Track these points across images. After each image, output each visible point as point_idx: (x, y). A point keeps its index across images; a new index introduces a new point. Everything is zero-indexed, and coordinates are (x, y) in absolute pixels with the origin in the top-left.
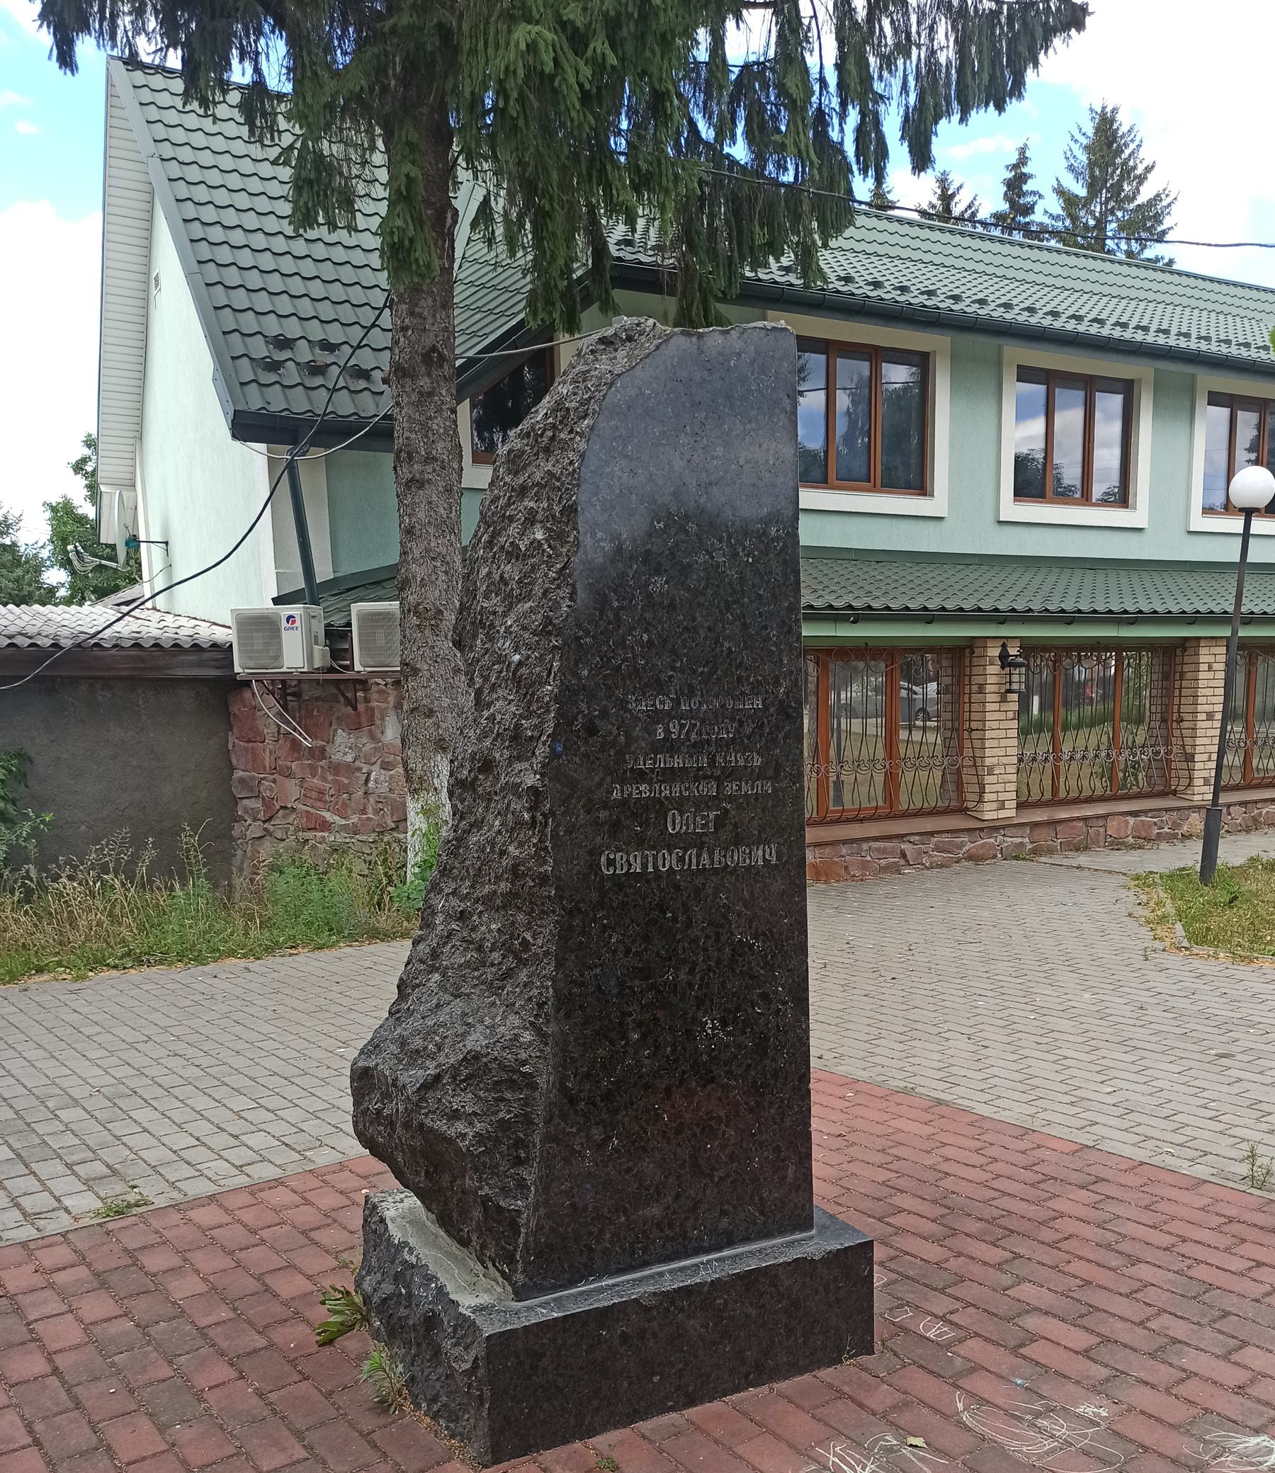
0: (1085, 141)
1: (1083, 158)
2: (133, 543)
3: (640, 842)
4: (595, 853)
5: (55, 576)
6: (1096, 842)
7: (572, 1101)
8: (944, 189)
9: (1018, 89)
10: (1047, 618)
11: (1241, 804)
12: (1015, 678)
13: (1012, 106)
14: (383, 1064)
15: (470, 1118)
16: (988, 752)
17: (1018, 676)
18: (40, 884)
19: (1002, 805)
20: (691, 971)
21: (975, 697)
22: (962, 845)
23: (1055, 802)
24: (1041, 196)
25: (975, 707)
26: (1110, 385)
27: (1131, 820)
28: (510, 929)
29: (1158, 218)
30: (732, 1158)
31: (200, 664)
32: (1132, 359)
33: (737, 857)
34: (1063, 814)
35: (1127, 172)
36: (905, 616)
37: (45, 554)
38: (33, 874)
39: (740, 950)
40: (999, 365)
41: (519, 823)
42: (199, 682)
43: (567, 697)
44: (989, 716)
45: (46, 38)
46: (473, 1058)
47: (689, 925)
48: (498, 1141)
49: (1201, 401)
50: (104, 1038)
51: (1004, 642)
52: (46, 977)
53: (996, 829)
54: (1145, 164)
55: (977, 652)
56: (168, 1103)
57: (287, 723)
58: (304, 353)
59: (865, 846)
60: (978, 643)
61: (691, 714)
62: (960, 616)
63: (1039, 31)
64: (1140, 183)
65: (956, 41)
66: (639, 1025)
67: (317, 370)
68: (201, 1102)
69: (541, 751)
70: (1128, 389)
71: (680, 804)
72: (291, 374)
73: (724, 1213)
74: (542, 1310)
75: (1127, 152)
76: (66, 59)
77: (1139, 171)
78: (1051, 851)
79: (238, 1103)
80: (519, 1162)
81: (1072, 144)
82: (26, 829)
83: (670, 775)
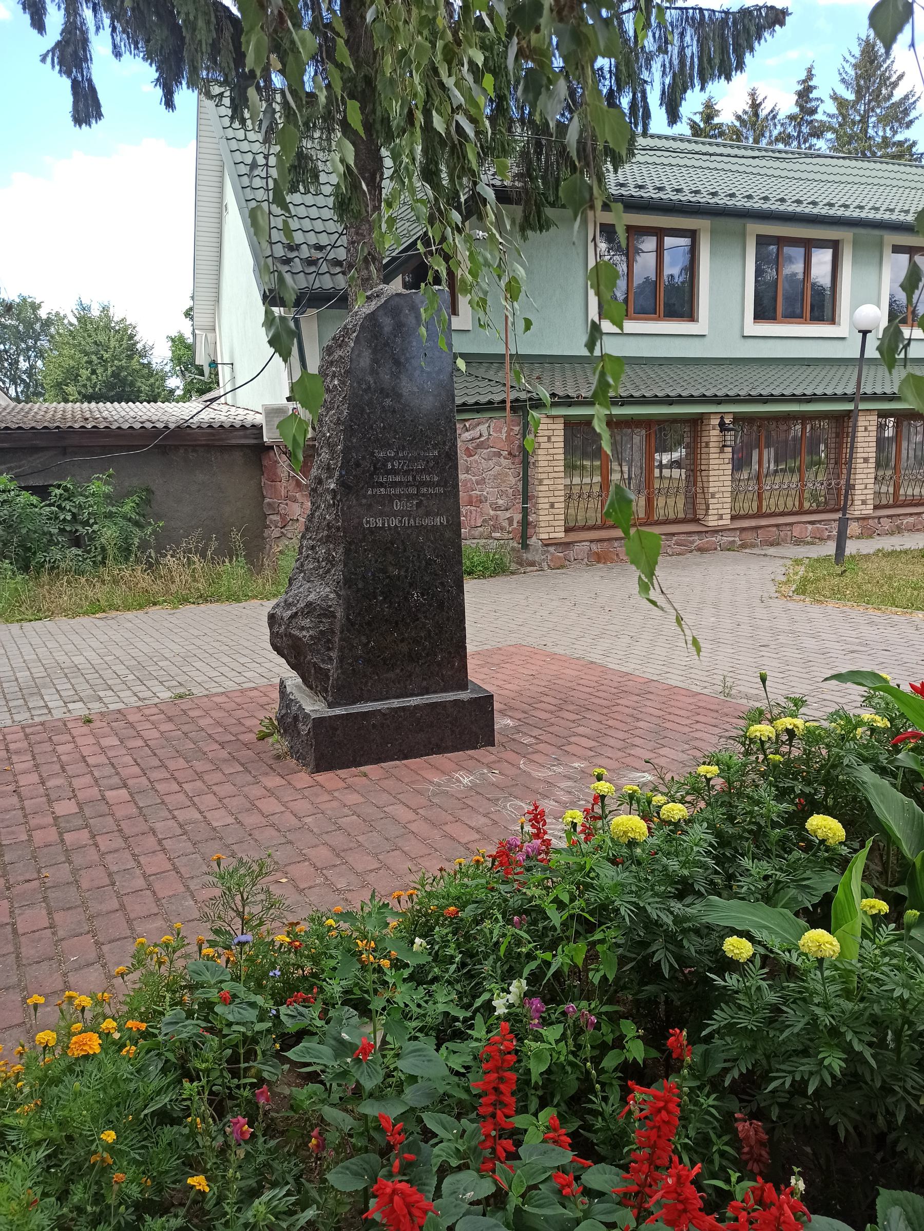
0: (853, 61)
1: (852, 72)
2: (214, 364)
3: (382, 514)
5: (175, 383)
6: (785, 541)
7: (353, 624)
8: (754, 100)
9: (740, 66)
10: (750, 399)
11: (888, 516)
12: (728, 438)
13: (737, 77)
14: (278, 611)
15: (308, 629)
16: (711, 484)
18: (157, 560)
19: (721, 517)
20: (406, 571)
21: (704, 450)
22: (694, 541)
23: (759, 515)
24: (822, 101)
25: (703, 456)
26: (822, 244)
27: (810, 527)
28: (328, 553)
29: (906, 112)
30: (427, 655)
31: (246, 437)
32: (835, 228)
34: (763, 522)
35: (884, 80)
36: (656, 401)
37: (167, 368)
38: (153, 555)
39: (429, 562)
40: (743, 236)
41: (329, 505)
42: (243, 447)
43: (346, 450)
44: (712, 462)
45: (159, 92)
46: (309, 604)
47: (405, 551)
48: (319, 639)
49: (887, 251)
50: (184, 634)
51: (722, 416)
52: (158, 607)
53: (717, 532)
54: (898, 74)
55: (705, 422)
56: (210, 660)
57: (293, 470)
58: (305, 252)
61: (404, 458)
63: (753, 29)
64: (894, 88)
65: (698, 41)
66: (382, 593)
67: (311, 262)
68: (226, 659)
69: (337, 474)
70: (835, 246)
71: (399, 497)
72: (297, 265)
73: (424, 679)
74: (338, 711)
75: (885, 66)
76: (169, 103)
77: (893, 79)
78: (753, 546)
79: (243, 660)
80: (329, 649)
81: (844, 64)
82: (149, 530)
83: (394, 484)
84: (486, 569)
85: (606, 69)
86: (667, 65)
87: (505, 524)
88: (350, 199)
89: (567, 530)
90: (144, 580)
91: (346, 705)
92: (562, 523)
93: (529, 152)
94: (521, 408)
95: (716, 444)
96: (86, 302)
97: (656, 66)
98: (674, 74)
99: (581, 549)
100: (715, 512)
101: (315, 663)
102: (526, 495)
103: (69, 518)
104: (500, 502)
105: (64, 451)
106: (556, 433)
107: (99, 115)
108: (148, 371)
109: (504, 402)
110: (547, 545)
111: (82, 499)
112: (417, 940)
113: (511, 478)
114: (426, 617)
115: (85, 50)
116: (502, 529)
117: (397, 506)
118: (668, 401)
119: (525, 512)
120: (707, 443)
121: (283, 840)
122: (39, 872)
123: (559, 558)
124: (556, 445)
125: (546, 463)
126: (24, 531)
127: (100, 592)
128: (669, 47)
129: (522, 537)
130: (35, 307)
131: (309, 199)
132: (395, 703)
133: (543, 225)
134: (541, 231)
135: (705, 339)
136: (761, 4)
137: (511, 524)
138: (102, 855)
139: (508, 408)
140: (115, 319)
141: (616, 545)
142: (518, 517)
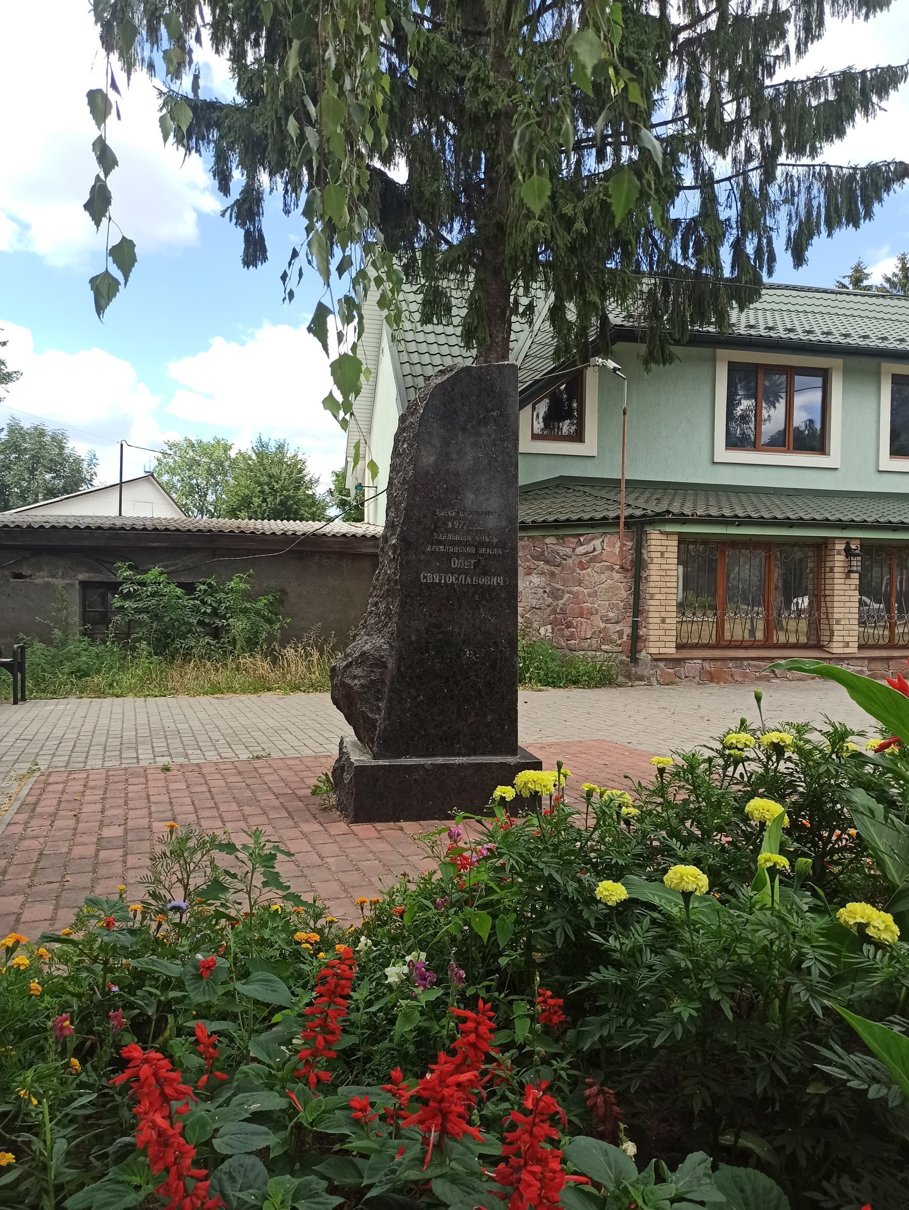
3: (439, 570)
4: (418, 573)
9: (869, 215)
10: (877, 526)
13: (865, 225)
16: (836, 610)
17: (856, 562)
19: (847, 645)
20: (460, 628)
25: (828, 581)
33: (484, 581)
44: (836, 587)
46: (363, 654)
48: (370, 689)
51: (848, 541)
59: (745, 663)
60: (830, 541)
62: (814, 524)
65: (825, 193)
71: (458, 555)
74: (381, 762)
80: (378, 699)
84: (591, 679)
85: (733, 220)
86: (794, 215)
87: (615, 637)
88: (476, 328)
89: (679, 647)
90: (263, 666)
91: (391, 757)
92: (674, 639)
93: (655, 294)
94: (638, 526)
95: (841, 570)
96: (265, 439)
97: (782, 214)
98: (801, 221)
99: (693, 667)
100: (841, 639)
101: (364, 712)
102: (637, 608)
103: (209, 611)
104: (611, 615)
105: (214, 552)
106: (669, 549)
107: (265, 259)
108: (312, 501)
109: (618, 517)
110: (656, 660)
111: (223, 595)
112: (363, 938)
113: (623, 592)
114: (477, 676)
115: (258, 206)
116: (612, 642)
117: (455, 563)
118: (789, 523)
119: (635, 626)
120: (832, 569)
121: (299, 874)
122: (64, 877)
123: (669, 674)
124: (669, 561)
125: (658, 578)
126: (166, 619)
127: (220, 677)
128: (796, 199)
129: (631, 651)
130: (227, 448)
131: (439, 329)
132: (440, 760)
133: (667, 359)
134: (664, 364)
135: (838, 472)
136: (889, 160)
137: (621, 637)
138: (126, 869)
139: (622, 524)
140: (289, 455)
141: (730, 665)
142: (628, 631)
